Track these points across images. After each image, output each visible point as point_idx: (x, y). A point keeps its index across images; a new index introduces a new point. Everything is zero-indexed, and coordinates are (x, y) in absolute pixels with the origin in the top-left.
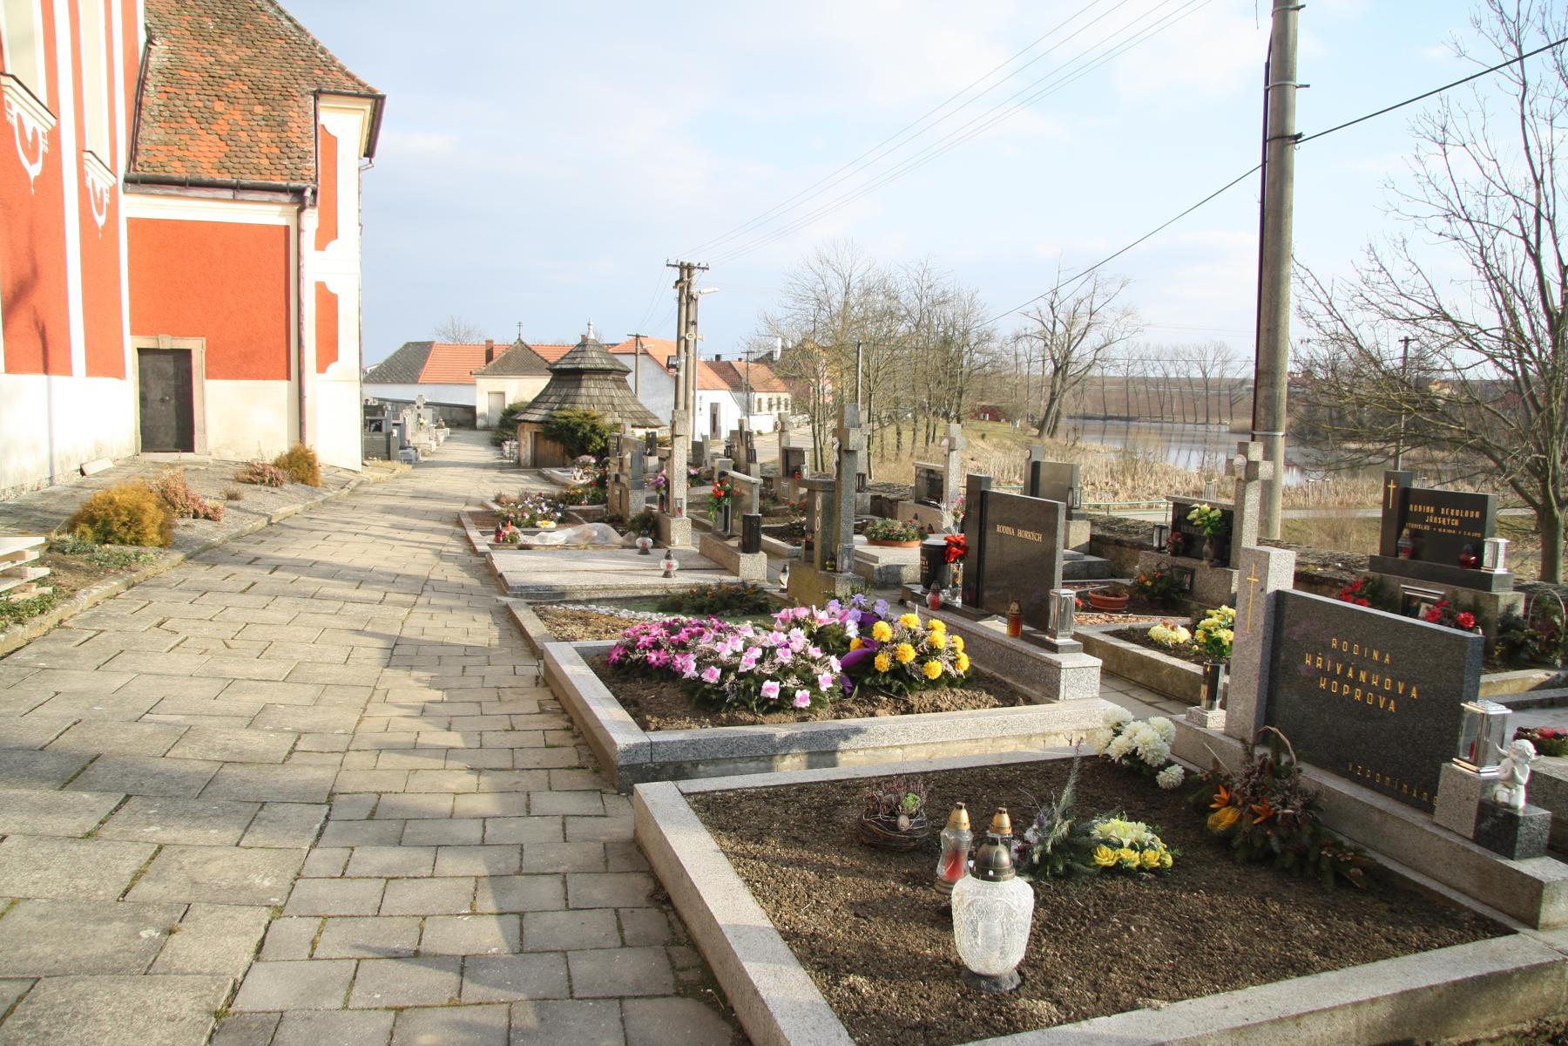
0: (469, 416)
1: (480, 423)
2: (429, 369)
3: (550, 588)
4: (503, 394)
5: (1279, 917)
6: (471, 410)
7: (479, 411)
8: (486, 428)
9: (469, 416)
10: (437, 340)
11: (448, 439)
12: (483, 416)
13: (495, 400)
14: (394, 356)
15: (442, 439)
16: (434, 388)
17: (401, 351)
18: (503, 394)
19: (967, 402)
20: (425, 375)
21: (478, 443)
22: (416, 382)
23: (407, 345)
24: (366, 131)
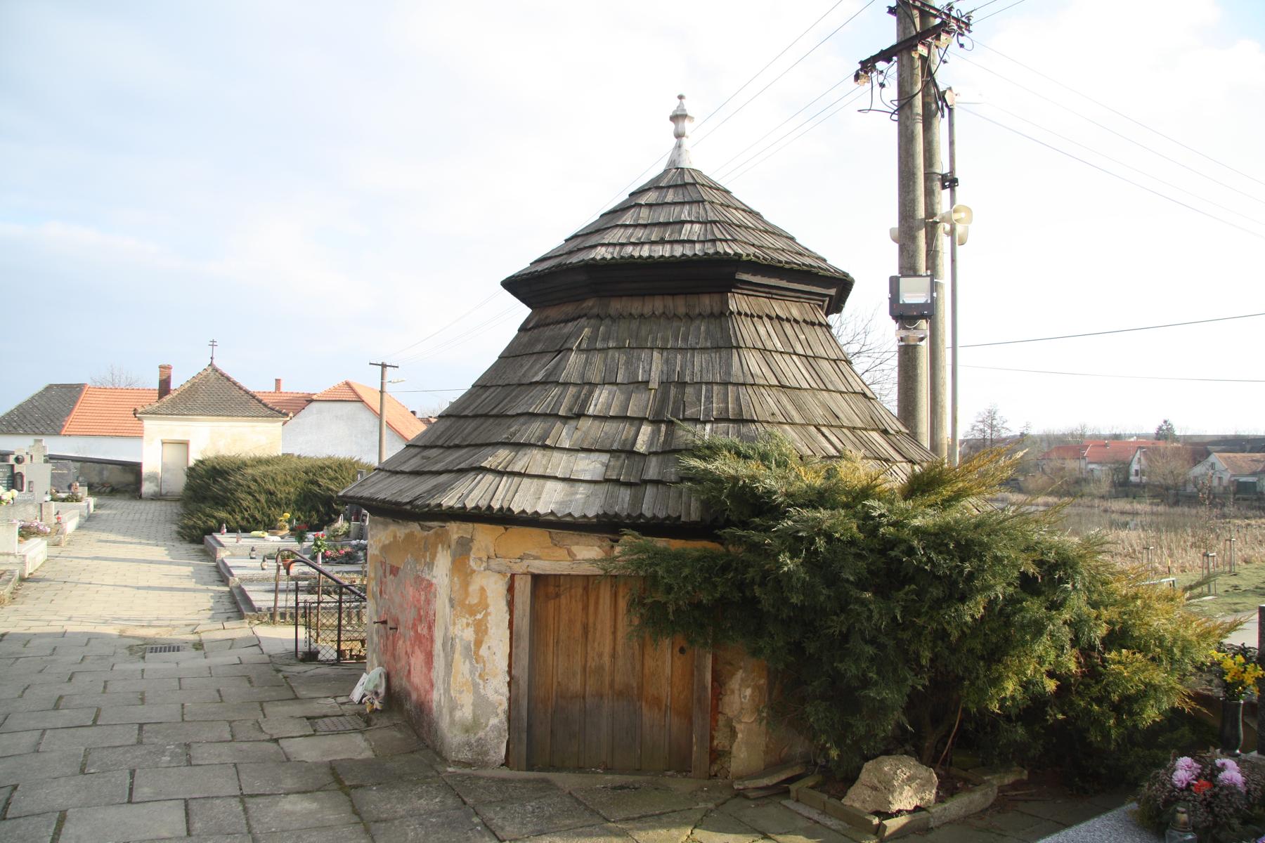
0: (130, 478)
1: (147, 488)
2: (78, 416)
3: (155, 641)
4: (185, 444)
5: (845, 637)
6: (134, 469)
7: (145, 470)
8: (157, 497)
9: (130, 478)
10: (89, 383)
11: (89, 521)
12: (153, 478)
13: (173, 454)
14: (31, 401)
15: (71, 525)
16: (81, 442)
17: (41, 395)
18: (185, 444)
19: (1045, 567)
20: (71, 424)
21: (147, 534)
22: (58, 434)
23: (49, 388)
24: (528, 530)
